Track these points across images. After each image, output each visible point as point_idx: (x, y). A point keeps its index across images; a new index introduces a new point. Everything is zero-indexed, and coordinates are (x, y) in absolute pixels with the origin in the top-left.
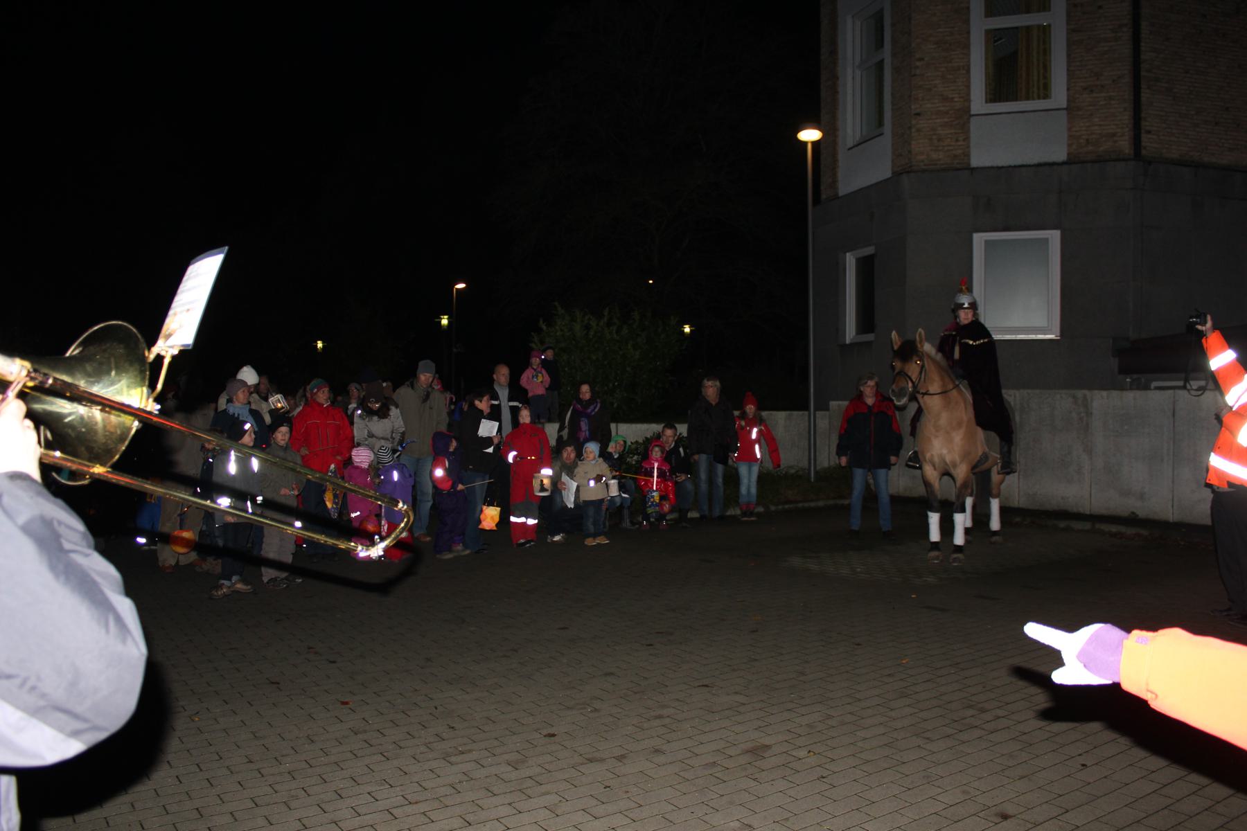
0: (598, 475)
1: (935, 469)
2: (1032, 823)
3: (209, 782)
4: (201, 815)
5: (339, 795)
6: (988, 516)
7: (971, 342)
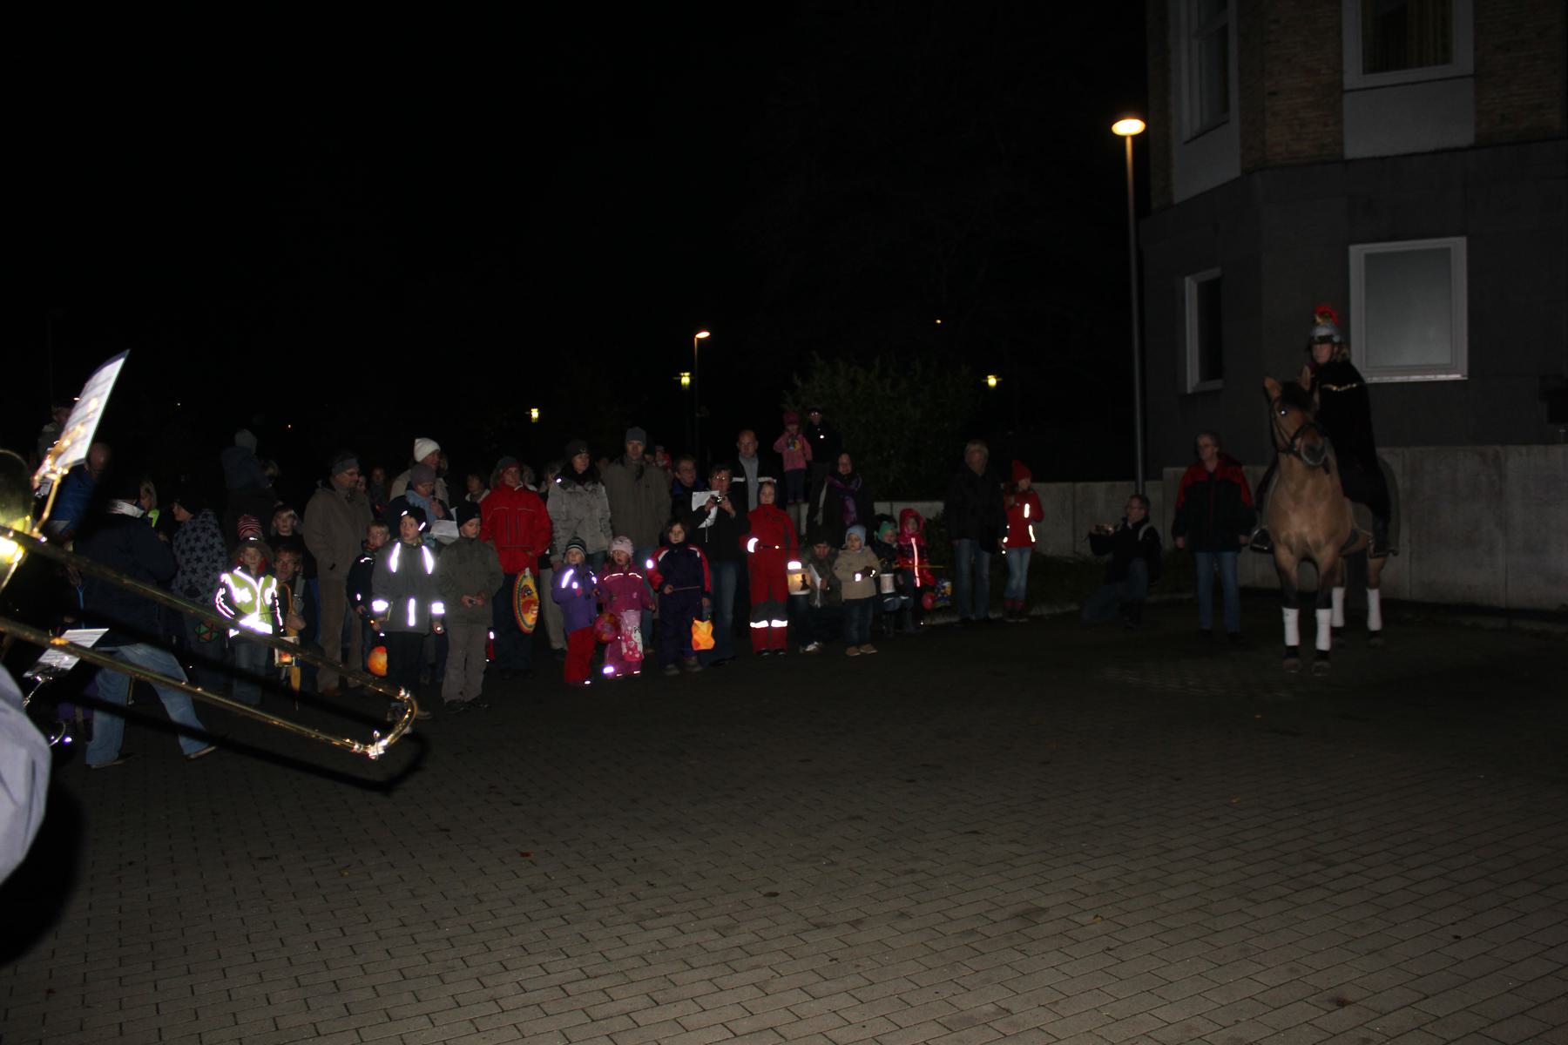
0: (867, 567)
1: (1292, 552)
2: (1377, 1012)
3: (352, 948)
4: (338, 989)
5: (504, 966)
6: (1365, 612)
7: (1335, 388)
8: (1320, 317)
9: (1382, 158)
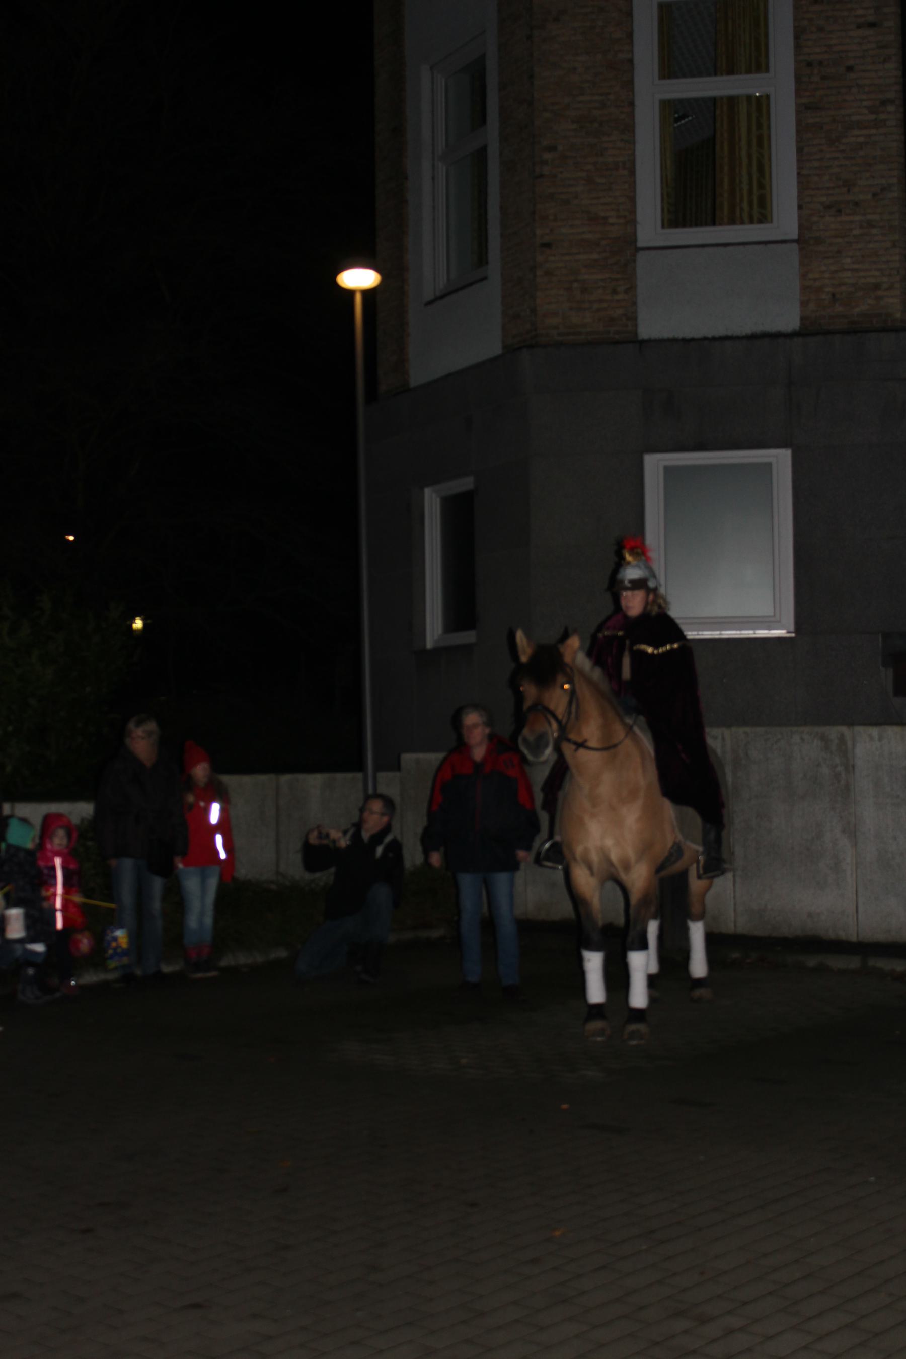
1: (592, 874)
7: (650, 650)
8: (630, 555)
9: (685, 341)
